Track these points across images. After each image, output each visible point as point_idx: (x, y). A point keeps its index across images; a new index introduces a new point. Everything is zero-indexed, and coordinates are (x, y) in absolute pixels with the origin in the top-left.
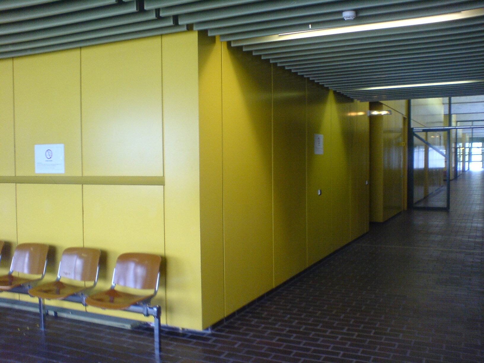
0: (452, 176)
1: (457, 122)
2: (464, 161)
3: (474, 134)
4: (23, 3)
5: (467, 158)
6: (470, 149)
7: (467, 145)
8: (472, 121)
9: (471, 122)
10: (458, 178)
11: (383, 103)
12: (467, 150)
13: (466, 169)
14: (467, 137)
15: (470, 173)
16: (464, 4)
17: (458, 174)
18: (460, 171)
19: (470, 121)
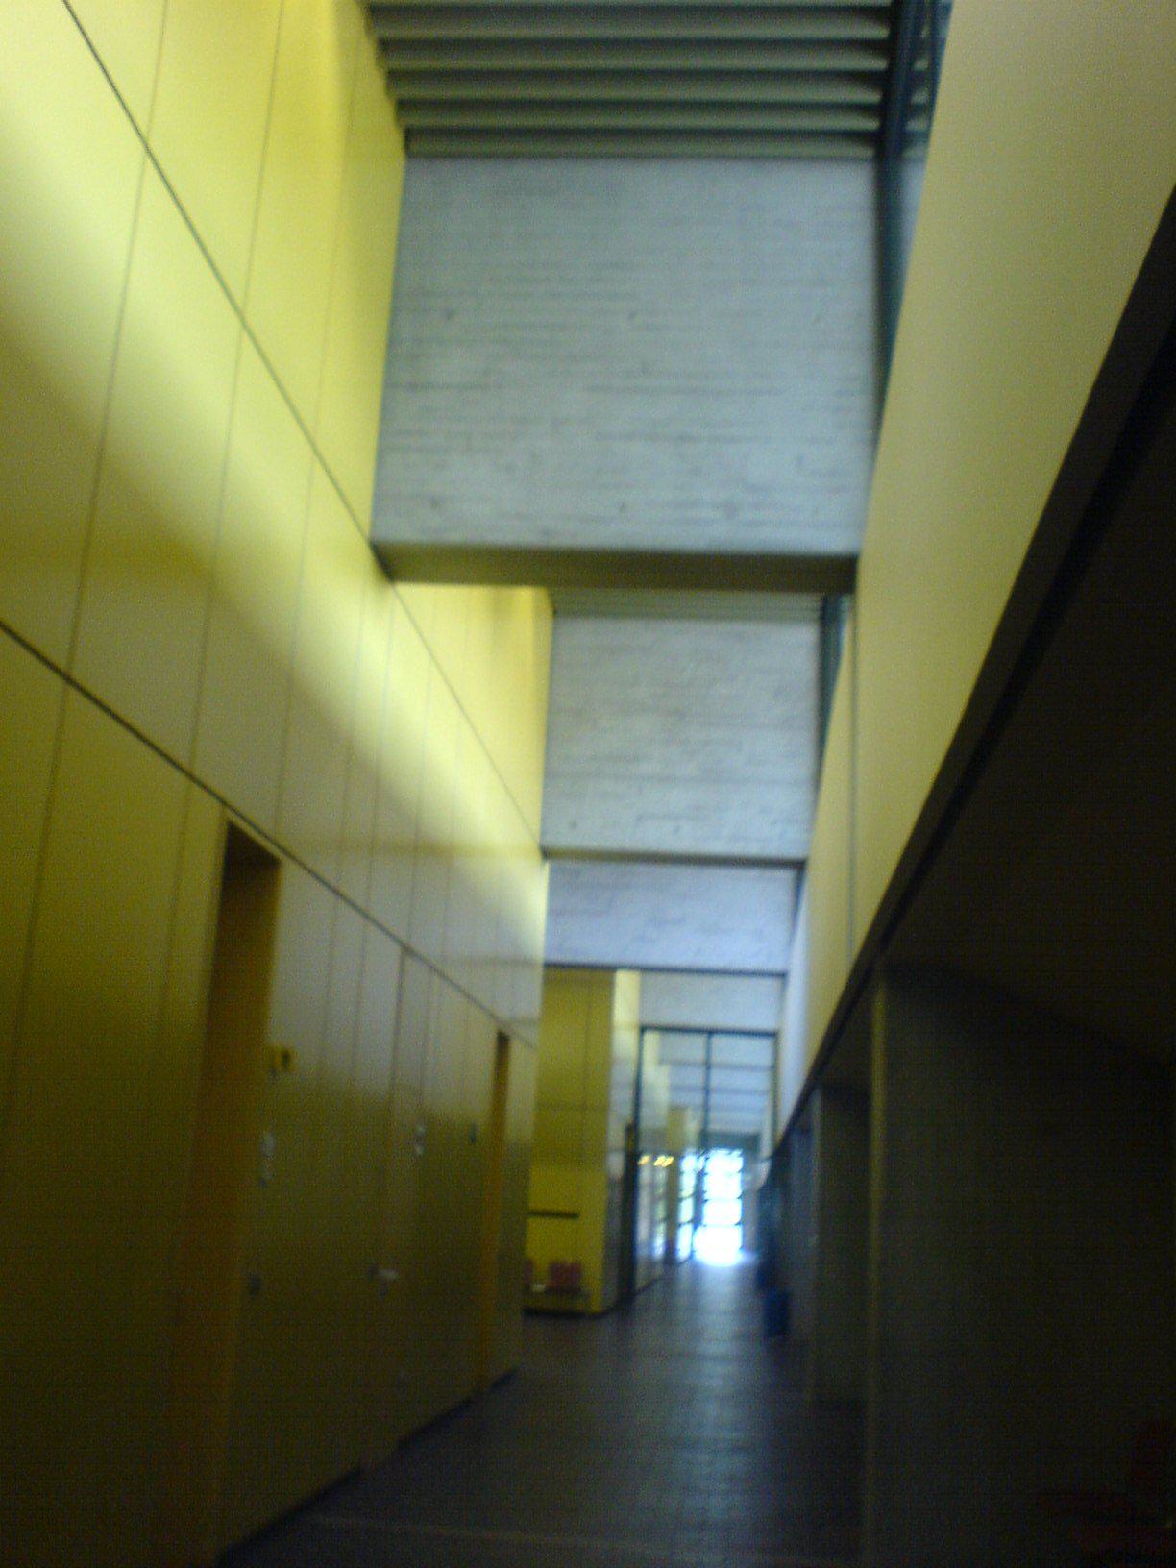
0: (597, 1286)
1: (643, 1029)
2: (672, 1222)
3: (714, 1115)
4: (874, 1175)
5: (686, 1211)
6: (701, 1175)
7: (690, 1164)
8: (711, 1032)
9: (699, 1041)
10: (640, 1300)
11: (608, 957)
12: (688, 1184)
13: (683, 1252)
14: (692, 1127)
15: (696, 1270)
16: (419, 136)
17: (640, 1282)
18: (651, 1263)
19: (699, 1031)
